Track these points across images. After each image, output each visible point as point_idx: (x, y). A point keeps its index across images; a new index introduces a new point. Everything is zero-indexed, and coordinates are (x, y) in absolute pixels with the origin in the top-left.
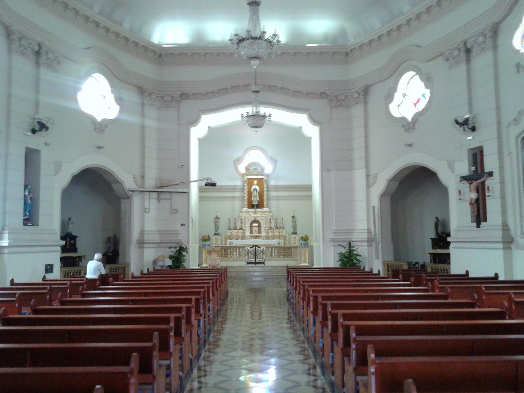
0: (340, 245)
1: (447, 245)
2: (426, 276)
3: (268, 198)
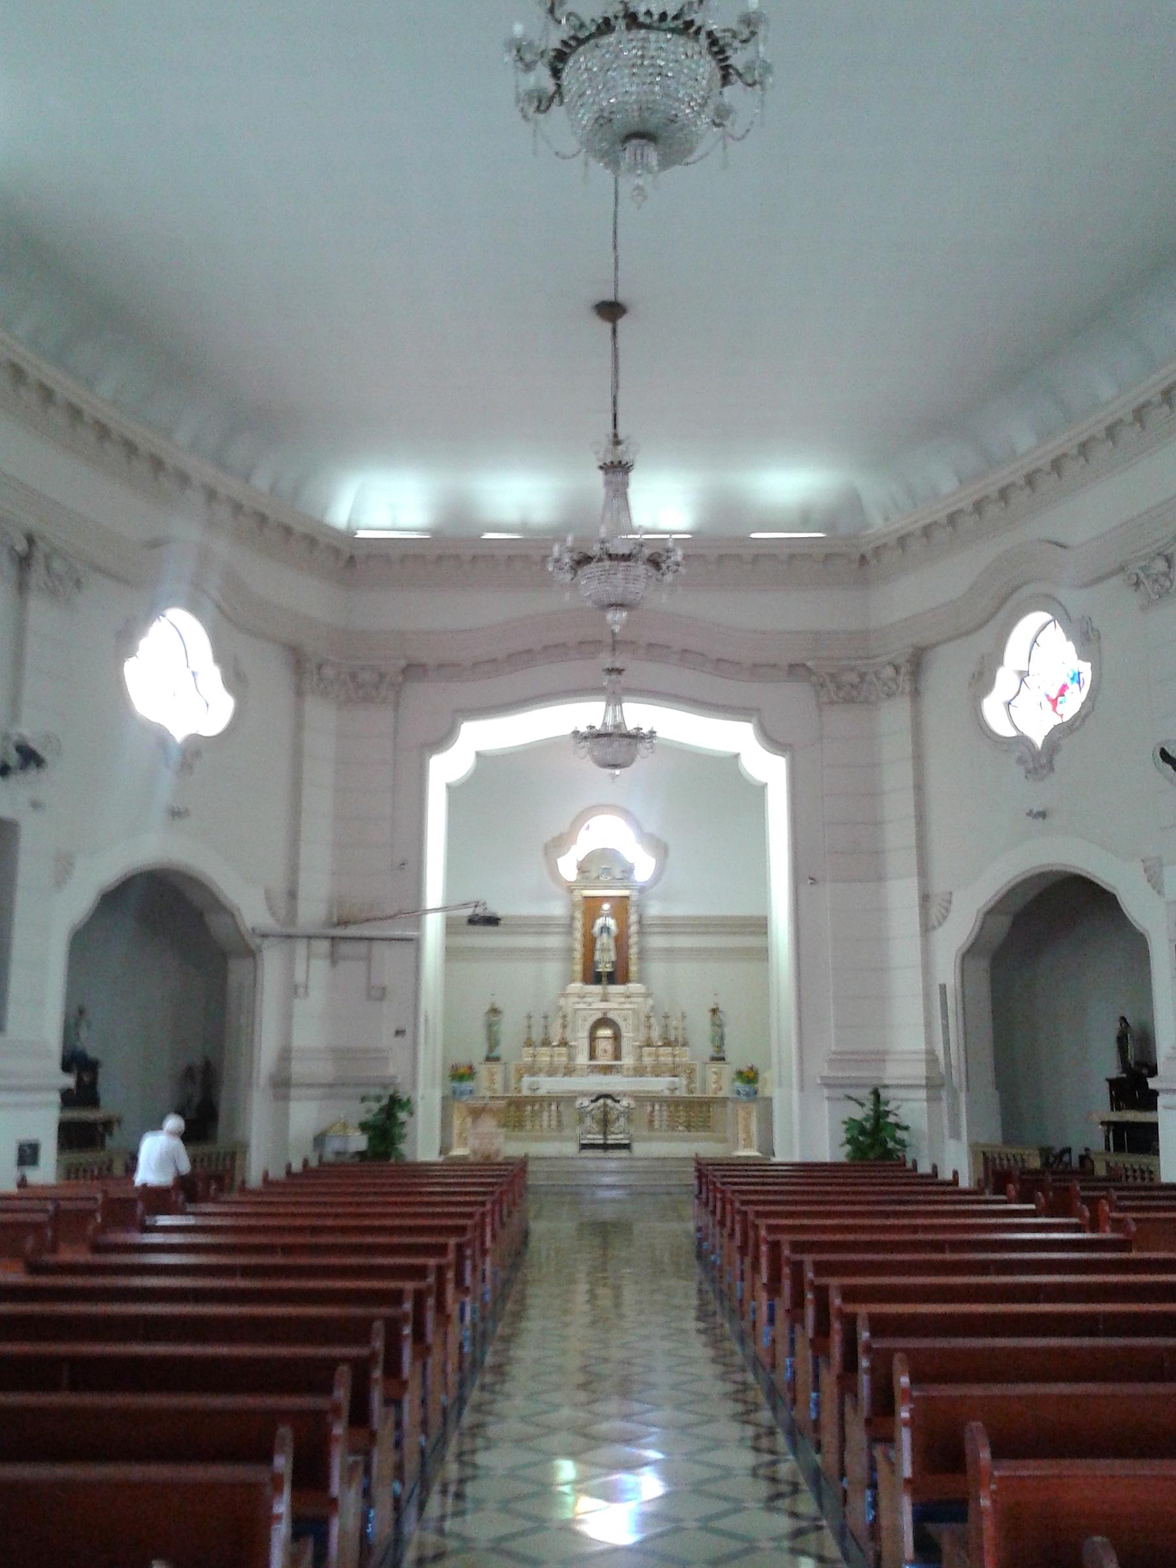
0: (850, 1098)
1: (1149, 1101)
2: (1083, 1189)
3: (642, 953)
